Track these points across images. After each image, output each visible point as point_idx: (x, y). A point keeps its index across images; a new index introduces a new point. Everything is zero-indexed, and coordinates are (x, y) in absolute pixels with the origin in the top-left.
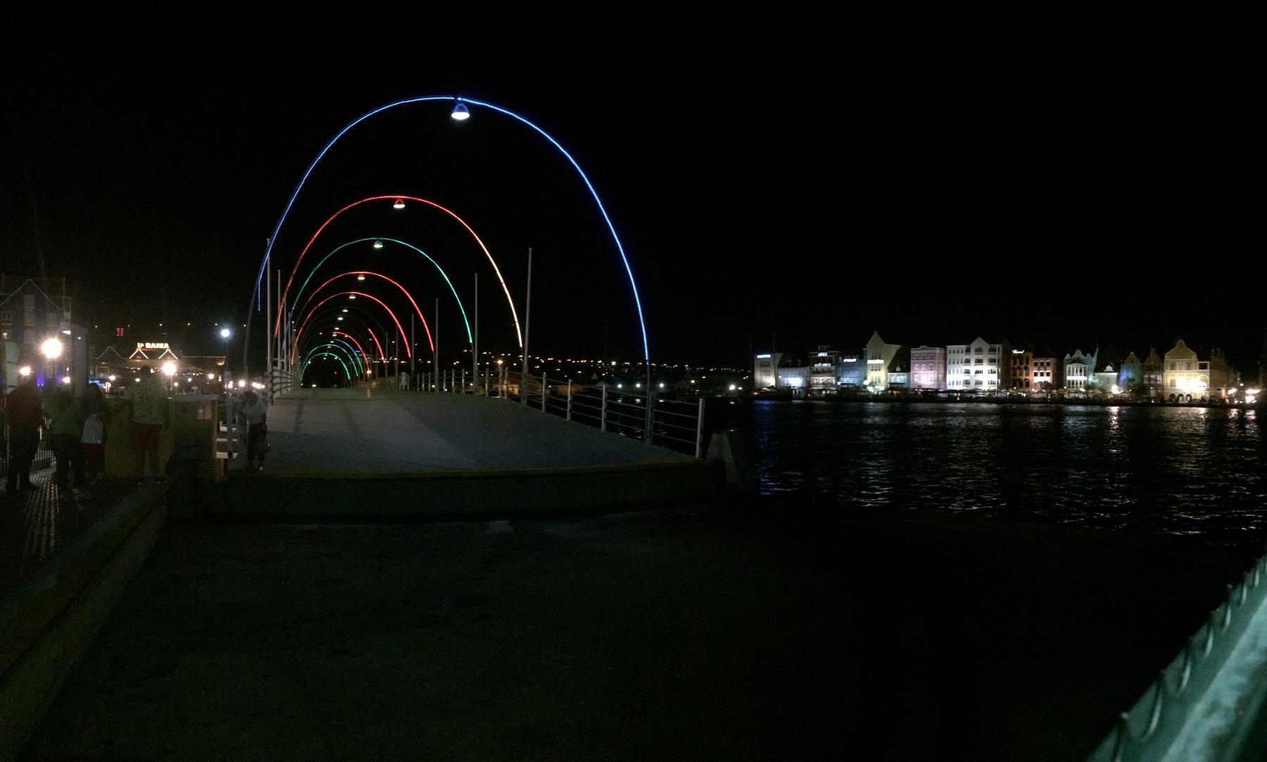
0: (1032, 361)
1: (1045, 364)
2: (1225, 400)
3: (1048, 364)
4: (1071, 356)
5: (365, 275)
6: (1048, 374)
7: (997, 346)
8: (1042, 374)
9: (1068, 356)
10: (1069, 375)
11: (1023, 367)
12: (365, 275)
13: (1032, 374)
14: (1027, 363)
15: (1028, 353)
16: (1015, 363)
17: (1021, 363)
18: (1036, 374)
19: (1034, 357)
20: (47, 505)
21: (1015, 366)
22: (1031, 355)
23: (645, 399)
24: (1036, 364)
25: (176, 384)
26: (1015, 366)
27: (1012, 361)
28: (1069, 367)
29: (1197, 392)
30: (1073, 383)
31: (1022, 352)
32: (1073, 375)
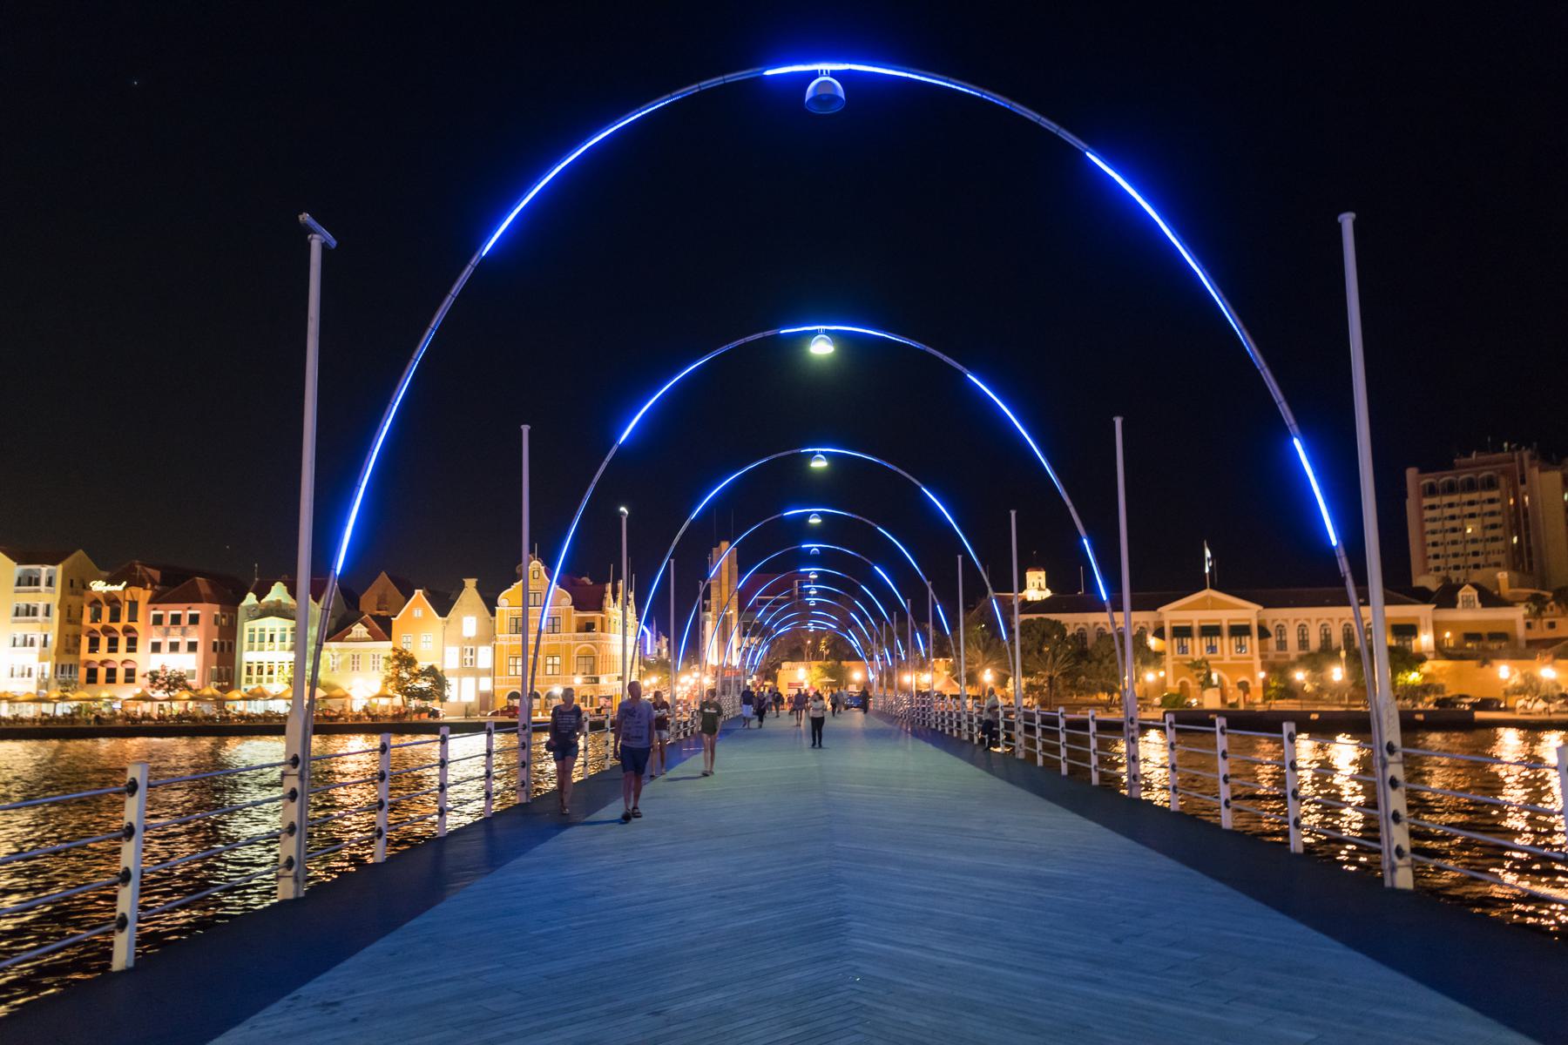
0: (146, 613)
1: (185, 621)
2: (1362, 756)
3: (194, 620)
4: (259, 598)
5: (821, 514)
6: (192, 647)
7: (44, 570)
8: (174, 647)
9: (251, 599)
10: (251, 649)
11: (118, 627)
12: (821, 514)
13: (143, 646)
14: (133, 618)
15: (134, 589)
16: (96, 616)
17: (115, 617)
18: (156, 647)
19: (155, 600)
20: (1473, 861)
21: (97, 627)
22: (143, 595)
23: (1374, 784)
24: (158, 620)
25: (578, 733)
26: (97, 627)
27: (88, 611)
28: (248, 627)
29: (1157, 734)
30: (260, 669)
31: (120, 588)
32: (261, 649)
